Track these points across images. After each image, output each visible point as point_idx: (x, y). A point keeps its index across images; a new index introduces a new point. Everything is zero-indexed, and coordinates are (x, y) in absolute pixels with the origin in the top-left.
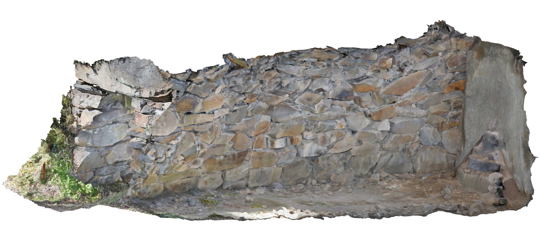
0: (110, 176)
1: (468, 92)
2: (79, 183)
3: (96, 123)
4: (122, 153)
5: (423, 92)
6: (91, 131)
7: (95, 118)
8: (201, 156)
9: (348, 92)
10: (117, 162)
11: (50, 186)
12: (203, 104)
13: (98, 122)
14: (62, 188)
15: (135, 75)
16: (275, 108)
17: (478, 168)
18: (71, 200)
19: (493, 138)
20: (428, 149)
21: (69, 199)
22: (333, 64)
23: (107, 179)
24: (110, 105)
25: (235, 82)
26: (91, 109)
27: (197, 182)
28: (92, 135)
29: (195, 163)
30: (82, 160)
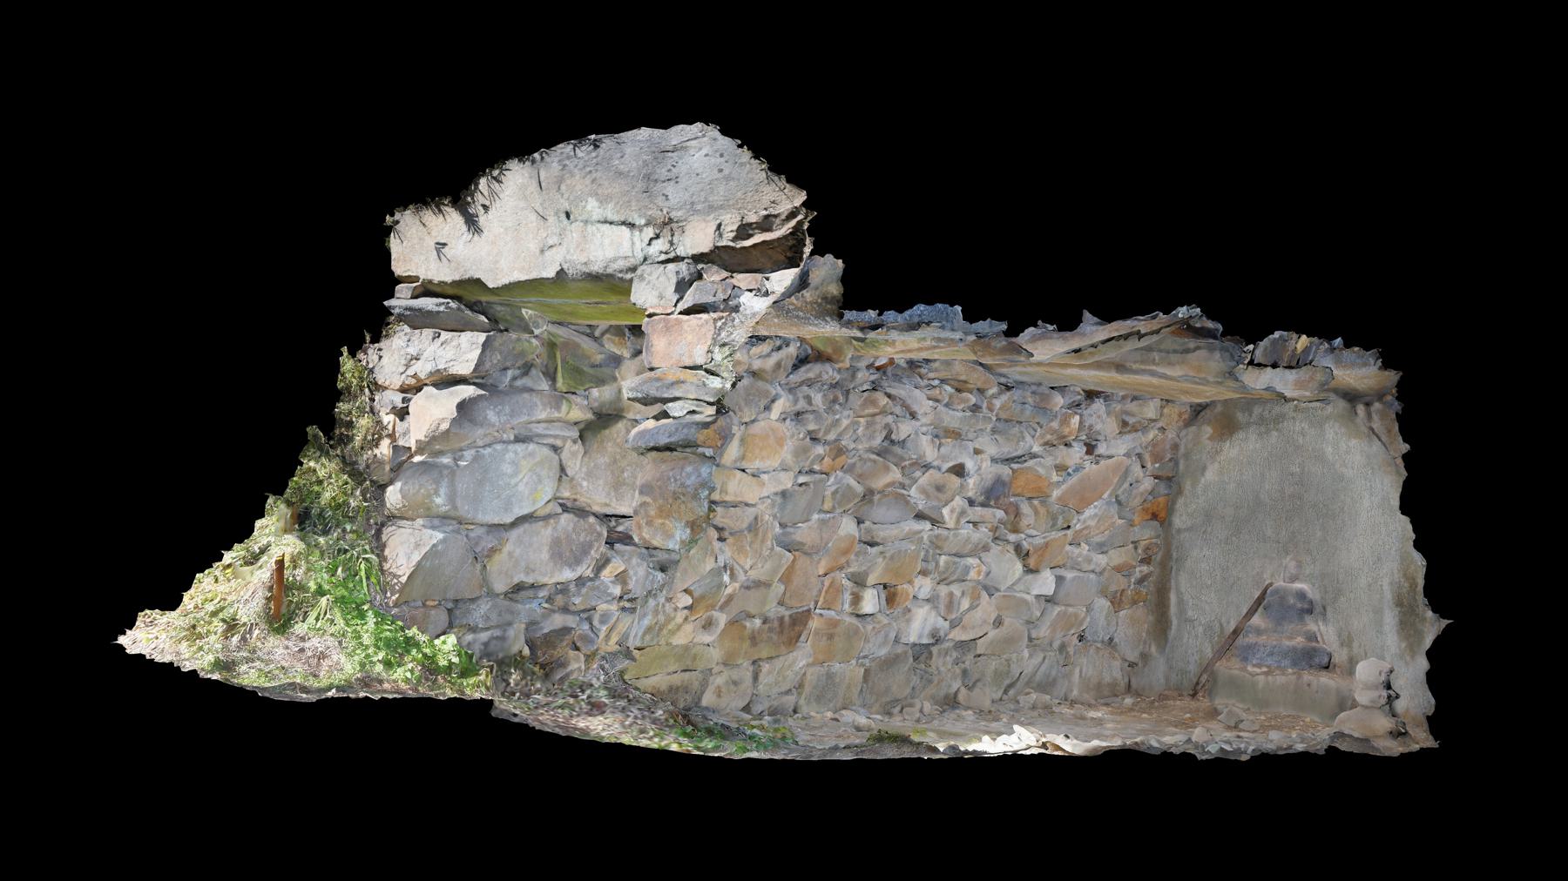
0: (497, 633)
1: (1178, 521)
2: (410, 633)
3: (467, 424)
4: (531, 558)
6: (446, 460)
7: (462, 406)
8: (722, 609)
10: (519, 588)
11: (303, 639)
13: (473, 421)
14: (350, 644)
15: (647, 177)
16: (876, 497)
17: (1286, 662)
18: (386, 686)
19: (1301, 595)
21: (381, 682)
23: (486, 644)
24: (510, 373)
25: (809, 399)
26: (447, 381)
27: (704, 684)
28: (452, 471)
30: (416, 557)
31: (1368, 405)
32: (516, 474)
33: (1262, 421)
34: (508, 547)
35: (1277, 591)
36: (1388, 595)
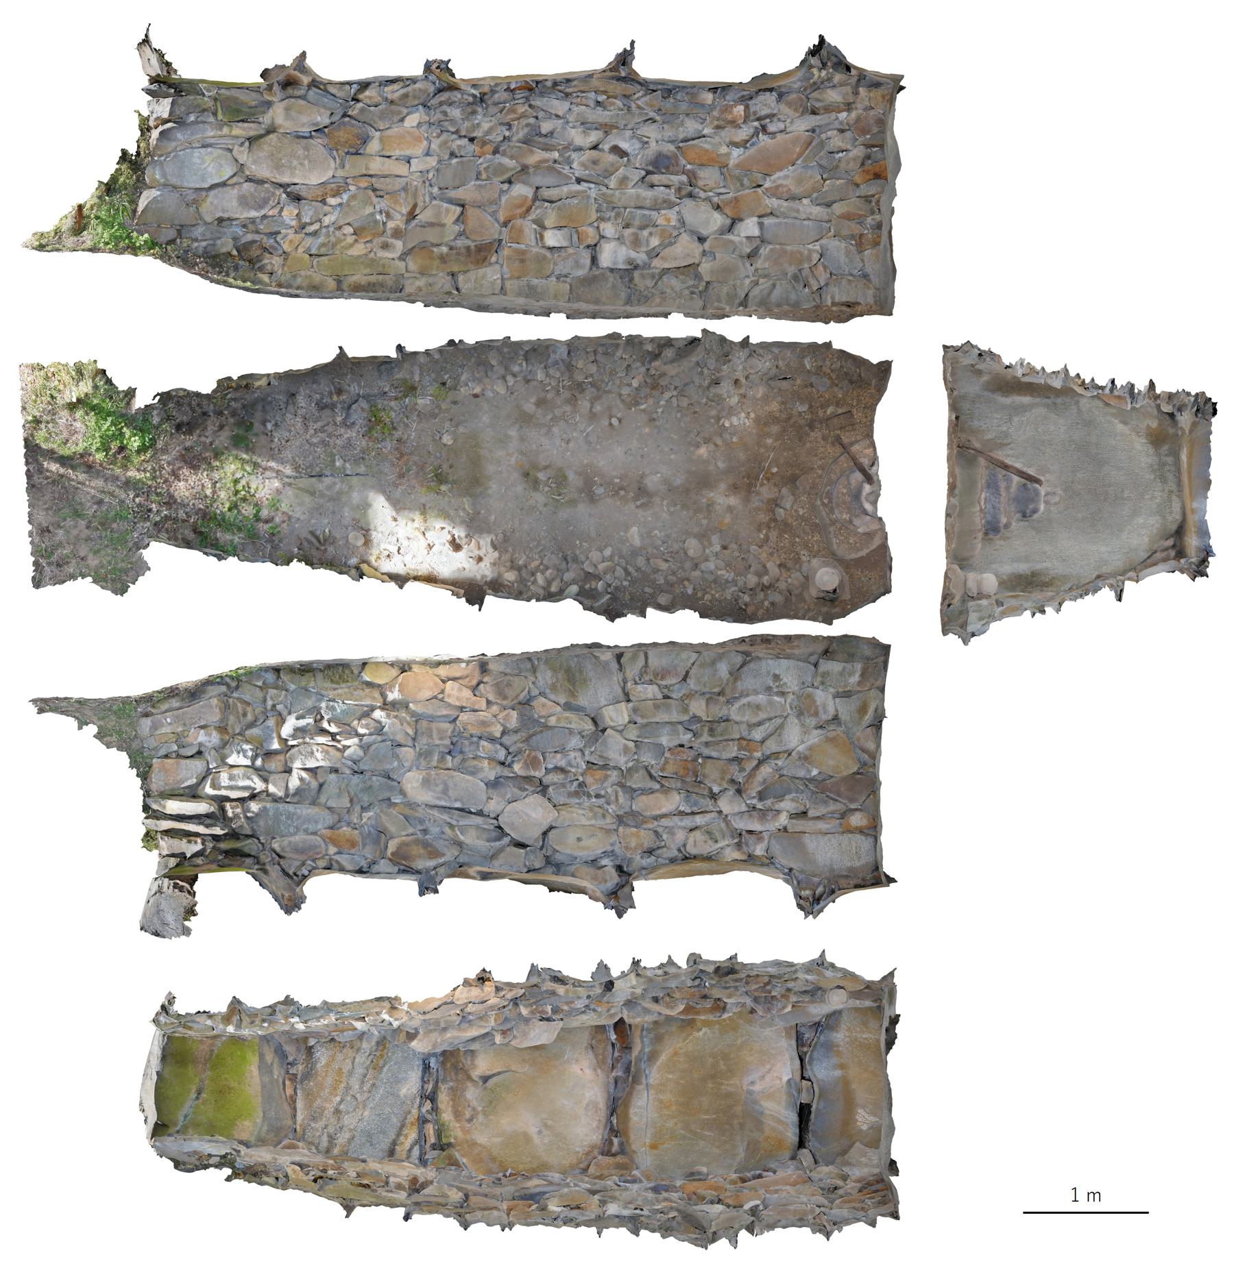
5: (810, 172)
9: (667, 157)
12: (381, 140)
13: (169, 139)
16: (531, 170)
19: (1035, 511)
20: (844, 282)
22: (633, 106)
25: (445, 114)
29: (385, 246)
31: (1174, 546)
32: (203, 163)
33: (1162, 465)
34: (209, 200)
35: (1037, 493)
36: (1039, 566)
